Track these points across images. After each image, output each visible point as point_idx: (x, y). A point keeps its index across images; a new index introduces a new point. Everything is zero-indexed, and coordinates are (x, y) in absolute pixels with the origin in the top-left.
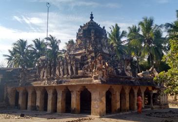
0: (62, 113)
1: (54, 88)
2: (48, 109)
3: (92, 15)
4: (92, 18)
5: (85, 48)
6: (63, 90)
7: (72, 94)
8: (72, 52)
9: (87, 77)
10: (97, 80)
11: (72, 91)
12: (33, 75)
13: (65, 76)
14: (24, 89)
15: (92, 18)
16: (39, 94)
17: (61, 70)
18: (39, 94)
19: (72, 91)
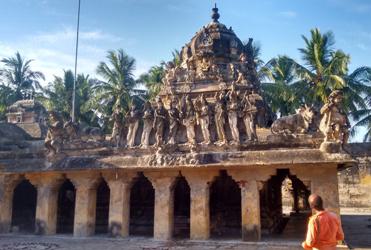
0: (91, 235)
1: (177, 174)
2: (156, 231)
3: (216, 10)
4: (216, 17)
5: (226, 80)
6: (211, 179)
7: (243, 189)
8: (185, 89)
9: (297, 146)
10: (337, 155)
11: (244, 182)
12: (95, 139)
13: (220, 143)
14: (59, 177)
15: (216, 17)
16: (118, 193)
17: (235, 132)
18: (118, 193)
19: (244, 182)
